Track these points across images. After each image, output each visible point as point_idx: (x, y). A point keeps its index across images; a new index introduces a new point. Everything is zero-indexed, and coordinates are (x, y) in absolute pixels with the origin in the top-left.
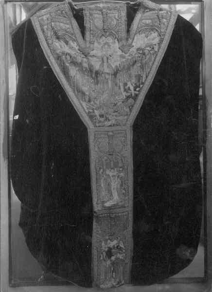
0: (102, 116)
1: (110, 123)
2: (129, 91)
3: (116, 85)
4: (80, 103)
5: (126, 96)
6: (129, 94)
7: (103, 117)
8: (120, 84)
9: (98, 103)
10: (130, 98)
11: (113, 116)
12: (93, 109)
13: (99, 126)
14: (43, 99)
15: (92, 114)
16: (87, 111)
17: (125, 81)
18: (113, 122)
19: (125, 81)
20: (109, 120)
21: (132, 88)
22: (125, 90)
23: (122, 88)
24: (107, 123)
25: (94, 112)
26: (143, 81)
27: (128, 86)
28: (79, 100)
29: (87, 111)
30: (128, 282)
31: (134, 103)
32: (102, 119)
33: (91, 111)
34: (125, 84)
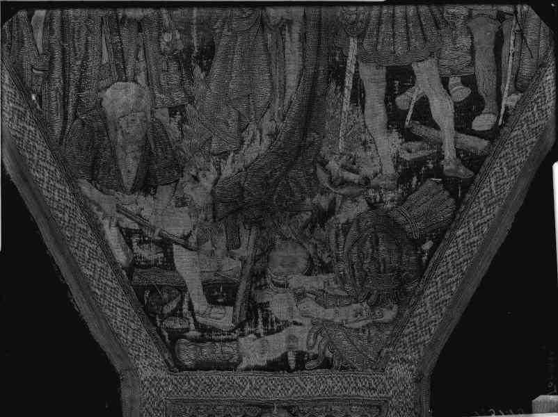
0: (219, 292)
1: (277, 345)
2: (421, 130)
3: (337, 73)
4: (76, 193)
5: (398, 160)
6: (415, 152)
7: (230, 302)
8: (367, 72)
9: (488, 46)
10: (429, 175)
11: (300, 296)
12: (165, 244)
13: (202, 366)
14: (6, 178)
15: (154, 278)
16: (121, 257)
17: (400, 49)
18: (303, 338)
19: (400, 49)
20: (273, 327)
21: (442, 110)
22: (395, 119)
23: (375, 94)
24: (253, 350)
25: (169, 263)
26: (526, 71)
27: (413, 95)
28: (71, 180)
29: (121, 257)
30: (232, 308)
31: (455, 219)
32: (223, 318)
33: (149, 254)
34: (399, 77)
